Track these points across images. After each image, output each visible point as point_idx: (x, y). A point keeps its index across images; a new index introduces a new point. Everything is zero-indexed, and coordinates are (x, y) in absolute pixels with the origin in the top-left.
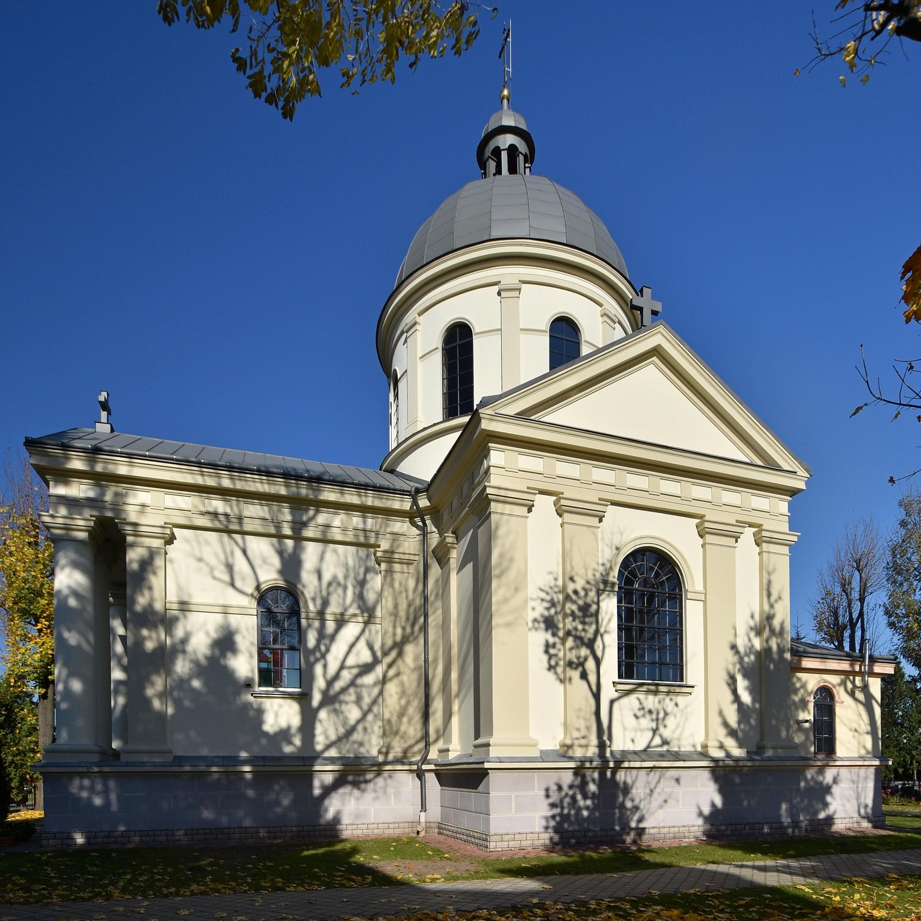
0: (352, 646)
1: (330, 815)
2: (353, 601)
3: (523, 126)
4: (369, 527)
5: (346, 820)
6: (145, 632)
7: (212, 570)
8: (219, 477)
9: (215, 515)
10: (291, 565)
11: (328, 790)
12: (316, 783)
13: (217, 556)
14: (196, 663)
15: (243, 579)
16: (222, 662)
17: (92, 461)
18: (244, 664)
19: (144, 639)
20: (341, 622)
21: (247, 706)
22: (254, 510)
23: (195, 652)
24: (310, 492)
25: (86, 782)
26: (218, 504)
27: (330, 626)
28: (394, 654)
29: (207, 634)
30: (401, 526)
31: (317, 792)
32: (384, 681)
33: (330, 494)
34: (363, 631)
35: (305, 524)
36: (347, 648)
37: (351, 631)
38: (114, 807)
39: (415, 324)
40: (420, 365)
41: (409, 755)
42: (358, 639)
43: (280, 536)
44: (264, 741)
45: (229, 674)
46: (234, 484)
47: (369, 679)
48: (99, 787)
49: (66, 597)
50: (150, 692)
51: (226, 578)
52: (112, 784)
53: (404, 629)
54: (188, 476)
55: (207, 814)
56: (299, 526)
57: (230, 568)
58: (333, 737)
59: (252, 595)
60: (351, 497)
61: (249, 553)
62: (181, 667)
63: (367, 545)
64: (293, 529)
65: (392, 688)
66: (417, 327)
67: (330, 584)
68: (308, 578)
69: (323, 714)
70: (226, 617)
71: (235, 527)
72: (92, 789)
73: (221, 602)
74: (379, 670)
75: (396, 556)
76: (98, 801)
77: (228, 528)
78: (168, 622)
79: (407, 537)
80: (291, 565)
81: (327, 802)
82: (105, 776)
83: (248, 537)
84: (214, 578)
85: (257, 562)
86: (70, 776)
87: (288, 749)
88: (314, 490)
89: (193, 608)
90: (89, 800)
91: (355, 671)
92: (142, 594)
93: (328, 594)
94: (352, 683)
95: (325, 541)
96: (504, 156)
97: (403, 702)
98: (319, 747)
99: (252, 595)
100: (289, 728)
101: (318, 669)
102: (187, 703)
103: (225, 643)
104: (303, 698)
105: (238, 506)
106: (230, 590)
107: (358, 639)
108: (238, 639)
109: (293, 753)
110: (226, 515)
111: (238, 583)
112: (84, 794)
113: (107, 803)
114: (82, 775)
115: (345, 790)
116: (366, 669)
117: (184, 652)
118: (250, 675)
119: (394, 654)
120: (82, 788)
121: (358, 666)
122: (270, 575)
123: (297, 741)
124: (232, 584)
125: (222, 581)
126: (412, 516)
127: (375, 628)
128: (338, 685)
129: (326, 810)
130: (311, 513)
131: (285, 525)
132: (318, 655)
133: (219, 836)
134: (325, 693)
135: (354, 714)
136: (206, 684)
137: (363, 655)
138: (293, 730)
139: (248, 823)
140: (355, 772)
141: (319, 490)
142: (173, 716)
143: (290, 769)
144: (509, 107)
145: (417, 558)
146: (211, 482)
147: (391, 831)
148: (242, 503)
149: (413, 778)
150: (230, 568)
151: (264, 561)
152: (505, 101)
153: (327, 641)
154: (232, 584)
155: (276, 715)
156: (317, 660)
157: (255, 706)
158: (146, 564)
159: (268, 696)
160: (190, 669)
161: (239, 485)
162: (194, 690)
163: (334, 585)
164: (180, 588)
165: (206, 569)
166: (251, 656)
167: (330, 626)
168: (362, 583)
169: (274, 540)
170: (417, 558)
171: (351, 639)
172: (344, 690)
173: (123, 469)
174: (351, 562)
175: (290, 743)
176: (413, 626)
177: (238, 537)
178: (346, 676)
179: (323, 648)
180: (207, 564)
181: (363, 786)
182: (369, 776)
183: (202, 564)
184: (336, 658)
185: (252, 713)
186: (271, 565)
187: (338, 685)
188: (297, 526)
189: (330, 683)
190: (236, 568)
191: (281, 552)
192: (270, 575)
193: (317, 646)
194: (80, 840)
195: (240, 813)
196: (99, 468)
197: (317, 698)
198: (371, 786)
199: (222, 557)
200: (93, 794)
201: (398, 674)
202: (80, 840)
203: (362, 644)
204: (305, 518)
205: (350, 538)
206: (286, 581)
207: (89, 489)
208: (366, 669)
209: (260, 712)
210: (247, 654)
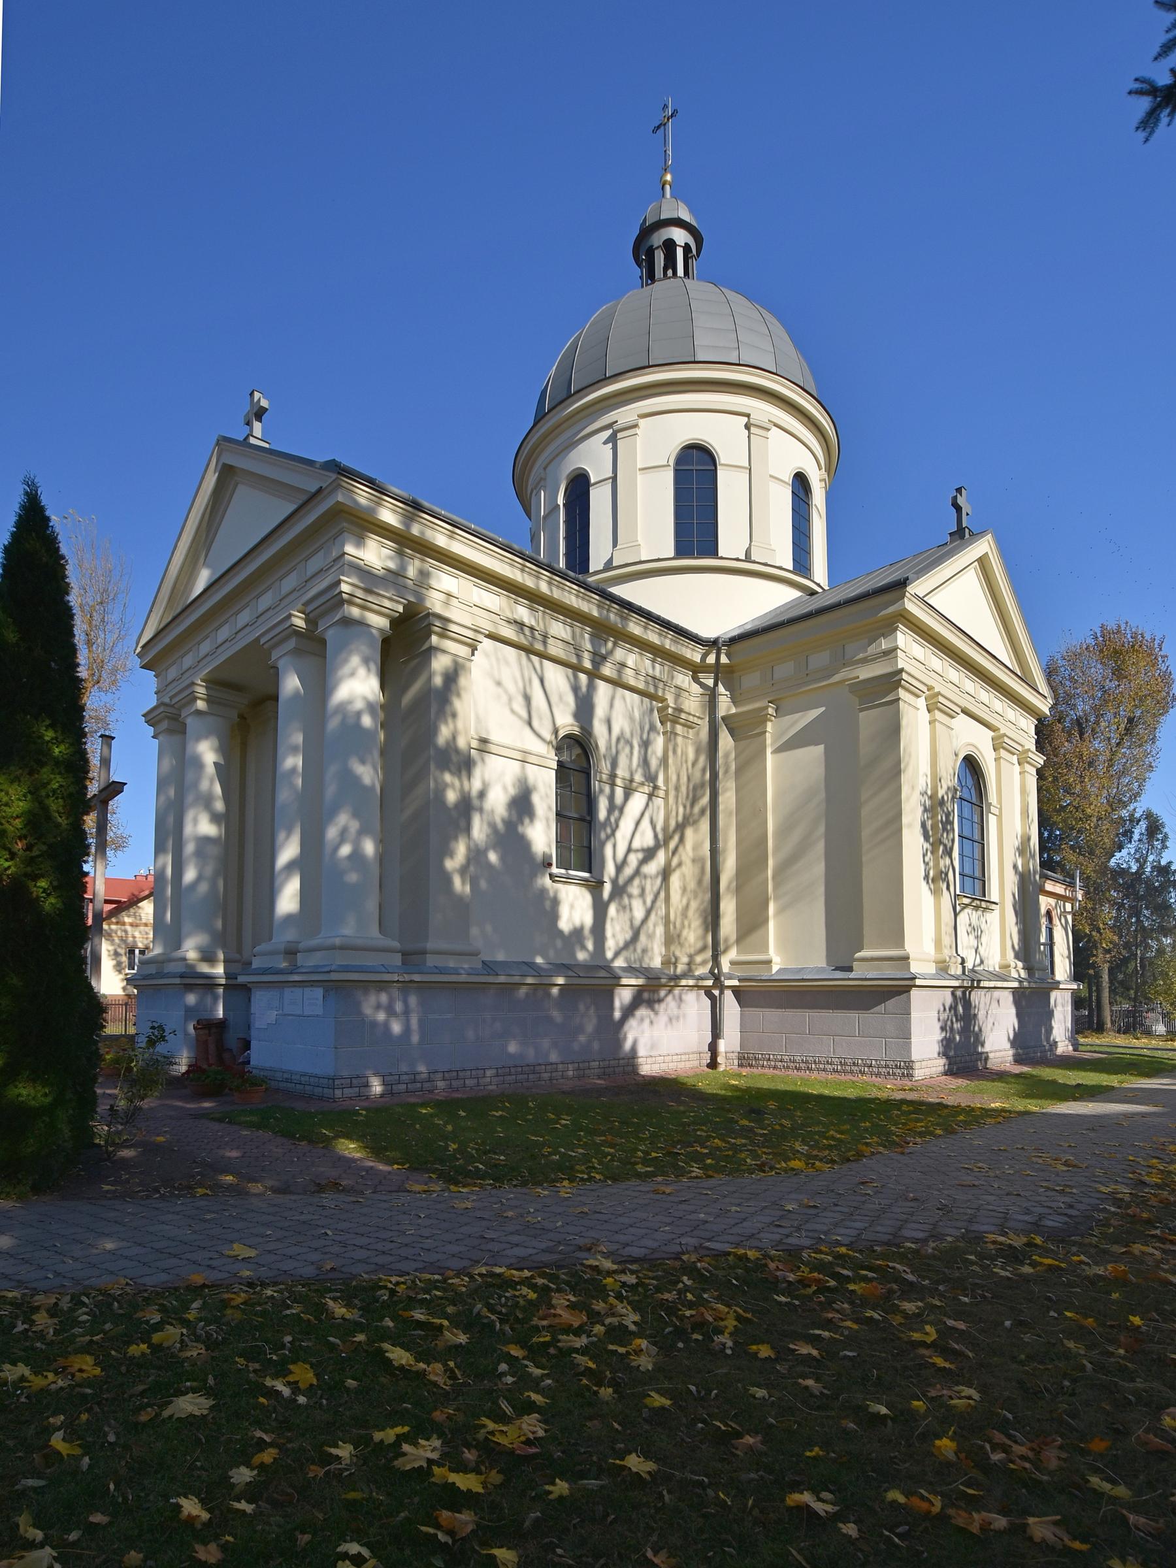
0: (638, 823)
1: (628, 1045)
2: (638, 765)
3: (694, 223)
4: (657, 674)
5: (642, 1052)
6: (448, 777)
7: (510, 700)
8: (538, 578)
9: (520, 625)
10: (584, 709)
11: (629, 1011)
12: (617, 1004)
13: (516, 683)
14: (492, 825)
15: (541, 719)
16: (520, 829)
17: (409, 519)
18: (542, 835)
19: (446, 786)
20: (628, 792)
21: (543, 891)
22: (559, 629)
23: (493, 811)
24: (618, 620)
25: (384, 998)
26: (523, 613)
27: (619, 793)
28: (676, 838)
29: (505, 788)
30: (683, 679)
31: (617, 1014)
32: (666, 873)
33: (635, 628)
34: (647, 805)
35: (604, 658)
36: (632, 826)
37: (637, 801)
38: (415, 1038)
39: (636, 426)
40: (640, 477)
41: (693, 967)
42: (642, 814)
43: (576, 668)
44: (559, 943)
45: (523, 844)
46: (551, 591)
47: (652, 868)
48: (399, 1007)
49: (359, 714)
50: (450, 864)
51: (524, 714)
52: (413, 1000)
53: (685, 807)
54: (507, 567)
55: (513, 1048)
56: (599, 659)
57: (527, 699)
58: (621, 944)
59: (550, 743)
60: (653, 637)
61: (547, 684)
62: (479, 830)
63: (652, 697)
64: (593, 661)
65: (675, 880)
66: (637, 430)
67: (618, 740)
68: (599, 729)
69: (612, 910)
70: (523, 768)
71: (539, 646)
72: (390, 1011)
73: (519, 745)
74: (661, 856)
75: (683, 716)
76: (396, 1028)
77: (531, 647)
78: (465, 765)
79: (689, 694)
80: (584, 709)
81: (626, 1027)
82: (406, 987)
83: (546, 663)
84: (513, 711)
85: (554, 699)
86: (366, 986)
87: (581, 956)
88: (621, 617)
89: (493, 748)
90: (386, 1025)
91: (640, 856)
92: (446, 723)
93: (617, 752)
94: (637, 872)
95: (617, 683)
96: (680, 253)
97: (685, 901)
98: (609, 954)
99: (550, 743)
100: (582, 928)
101: (608, 850)
102: (483, 884)
103: (522, 804)
104: (595, 887)
105: (544, 618)
106: (527, 730)
107: (642, 814)
108: (536, 799)
109: (585, 960)
110: (532, 629)
111: (535, 724)
112: (381, 1016)
113: (407, 1030)
114: (382, 986)
115: (642, 1012)
116: (649, 854)
117: (481, 810)
118: (547, 850)
119: (676, 838)
120: (378, 1007)
121: (643, 850)
122: (566, 722)
123: (590, 945)
124: (530, 724)
125: (520, 717)
126: (696, 670)
127: (659, 802)
128: (628, 871)
129: (625, 1038)
130: (610, 645)
131: (586, 655)
132: (609, 831)
133: (531, 1076)
134: (614, 882)
135: (639, 913)
136: (502, 858)
137: (645, 838)
138: (587, 932)
139: (554, 1057)
140: (653, 990)
141: (624, 619)
142: (289, 918)
143: (594, 983)
144: (672, 196)
145: (699, 722)
146: (530, 582)
147: (672, 1066)
148: (547, 617)
149: (698, 996)
150: (527, 699)
151: (561, 698)
152: (668, 187)
153: (616, 813)
154: (530, 724)
155: (572, 907)
156: (608, 838)
157: (551, 894)
158: (452, 677)
159: (567, 880)
160: (488, 836)
161: (557, 594)
162: (489, 865)
163: (622, 742)
164: (478, 720)
165: (505, 698)
166: (548, 826)
167: (619, 793)
168: (646, 744)
169: (570, 671)
170: (699, 722)
171: (637, 814)
172: (631, 879)
173: (440, 539)
174: (637, 715)
175: (584, 947)
176: (692, 805)
177: (535, 659)
178: (633, 860)
179: (612, 819)
180: (506, 691)
181: (656, 1006)
182: (662, 993)
183: (500, 690)
184: (624, 837)
185: (548, 904)
186: (567, 704)
187: (628, 871)
188: (598, 659)
189: (619, 868)
190: (534, 703)
191: (575, 689)
192: (566, 722)
193: (608, 818)
194: (377, 1087)
195: (546, 1043)
196: (415, 530)
197: (607, 888)
198: (663, 1006)
199: (521, 685)
200: (389, 1015)
201: (680, 865)
202: (377, 1087)
203: (645, 823)
204: (603, 651)
205: (641, 686)
206: (582, 728)
207: (391, 558)
208: (649, 854)
209: (556, 902)
210: (544, 822)
